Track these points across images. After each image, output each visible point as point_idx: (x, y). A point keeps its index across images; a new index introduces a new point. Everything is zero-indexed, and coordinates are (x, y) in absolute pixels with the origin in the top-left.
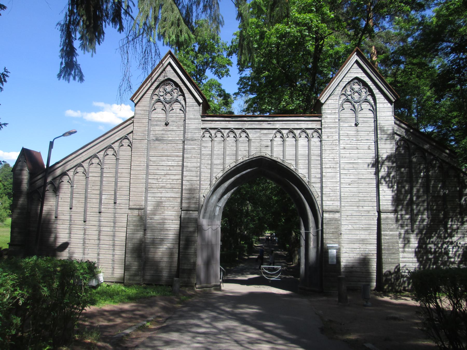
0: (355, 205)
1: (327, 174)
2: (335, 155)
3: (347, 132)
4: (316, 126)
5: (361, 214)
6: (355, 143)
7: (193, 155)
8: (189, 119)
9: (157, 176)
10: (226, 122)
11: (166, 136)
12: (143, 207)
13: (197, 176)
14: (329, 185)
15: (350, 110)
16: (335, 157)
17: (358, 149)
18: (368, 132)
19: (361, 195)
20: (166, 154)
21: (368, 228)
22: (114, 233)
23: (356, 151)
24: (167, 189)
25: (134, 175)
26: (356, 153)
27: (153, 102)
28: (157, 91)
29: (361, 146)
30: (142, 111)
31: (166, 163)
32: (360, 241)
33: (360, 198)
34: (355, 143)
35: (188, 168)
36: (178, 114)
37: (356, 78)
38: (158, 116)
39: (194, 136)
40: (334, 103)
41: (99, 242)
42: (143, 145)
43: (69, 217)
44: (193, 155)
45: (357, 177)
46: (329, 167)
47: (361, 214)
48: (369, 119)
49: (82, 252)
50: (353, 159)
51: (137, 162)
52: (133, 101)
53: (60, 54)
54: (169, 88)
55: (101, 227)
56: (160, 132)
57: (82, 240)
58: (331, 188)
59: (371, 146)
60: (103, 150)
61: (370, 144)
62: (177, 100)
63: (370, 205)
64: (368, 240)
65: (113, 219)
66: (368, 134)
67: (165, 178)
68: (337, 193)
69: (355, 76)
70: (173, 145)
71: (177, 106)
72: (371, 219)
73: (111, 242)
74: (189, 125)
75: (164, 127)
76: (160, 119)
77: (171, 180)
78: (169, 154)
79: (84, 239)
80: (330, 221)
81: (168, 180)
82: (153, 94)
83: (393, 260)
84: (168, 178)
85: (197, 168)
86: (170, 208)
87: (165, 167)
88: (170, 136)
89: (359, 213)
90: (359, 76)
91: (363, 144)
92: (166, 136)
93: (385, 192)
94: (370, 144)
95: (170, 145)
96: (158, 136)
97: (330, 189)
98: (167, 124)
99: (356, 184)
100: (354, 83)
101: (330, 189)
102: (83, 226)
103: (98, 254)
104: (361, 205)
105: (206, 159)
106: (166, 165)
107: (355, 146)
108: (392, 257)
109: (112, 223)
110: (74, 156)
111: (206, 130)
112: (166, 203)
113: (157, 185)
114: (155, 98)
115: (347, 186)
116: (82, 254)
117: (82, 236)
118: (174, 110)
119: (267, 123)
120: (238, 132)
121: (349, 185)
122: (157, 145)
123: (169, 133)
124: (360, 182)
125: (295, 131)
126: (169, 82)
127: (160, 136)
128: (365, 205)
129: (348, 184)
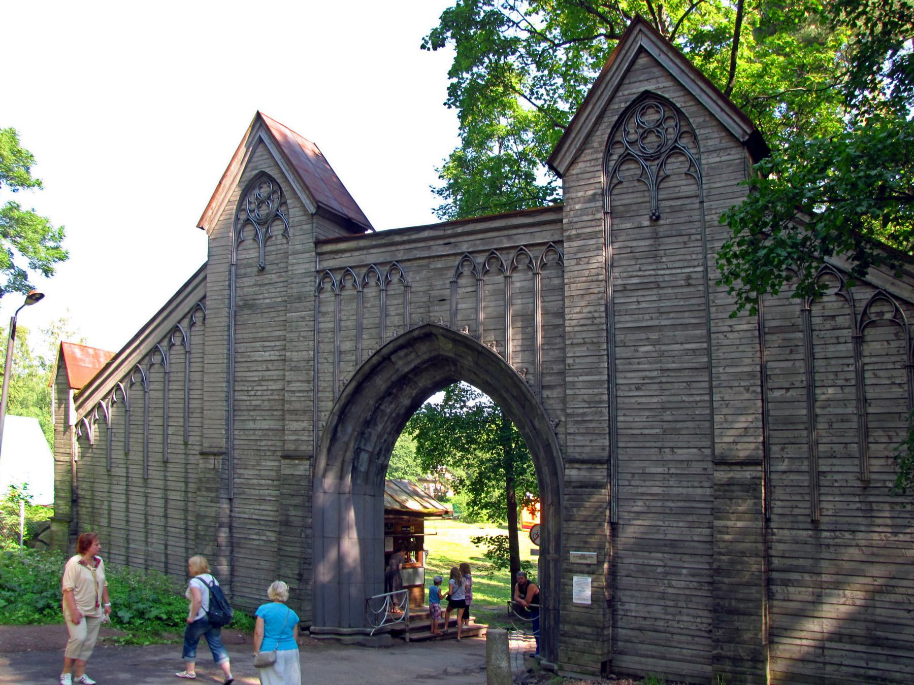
0: (653, 444)
1: (577, 360)
2: (597, 308)
3: (630, 244)
4: (552, 235)
5: (669, 469)
6: (652, 272)
7: (302, 334)
8: (294, 254)
9: (247, 384)
10: (361, 252)
11: (261, 297)
12: (224, 450)
13: (308, 382)
14: (583, 391)
15: (683, 176)
16: (596, 315)
17: (659, 287)
18: (686, 238)
19: (667, 416)
20: (260, 335)
21: (687, 511)
22: (186, 505)
23: (652, 295)
24: (263, 413)
25: (210, 385)
26: (654, 298)
27: (239, 226)
28: (246, 202)
29: (667, 278)
30: (220, 248)
31: (262, 356)
32: (665, 545)
33: (665, 425)
34: (652, 272)
35: (293, 364)
36: (279, 247)
37: (646, 95)
38: (248, 256)
39: (304, 290)
40: (592, 169)
41: (167, 522)
42: (220, 320)
43: (125, 470)
44: (302, 334)
45: (657, 366)
46: (582, 341)
47: (669, 469)
48: (688, 201)
49: (143, 539)
50: (647, 317)
51: (213, 357)
52: (202, 228)
53: (450, 68)
54: (652, 117)
55: (168, 493)
56: (250, 289)
57: (143, 517)
58: (586, 397)
59: (694, 276)
60: (165, 337)
61: (691, 270)
62: (675, 147)
63: (691, 445)
64: (686, 544)
65: (183, 475)
66: (685, 243)
67: (260, 388)
68: (601, 412)
69: (642, 89)
70: (273, 314)
71: (675, 165)
72: (696, 484)
73: (182, 522)
74: (295, 268)
75: (257, 278)
76: (250, 261)
77: (269, 393)
78: (265, 334)
79: (146, 515)
80: (581, 487)
81: (265, 393)
82: (611, 142)
83: (742, 606)
84: (265, 388)
85: (308, 361)
86: (268, 453)
87: (259, 364)
88: (266, 295)
89: (663, 466)
90: (651, 87)
91: (674, 271)
92: (261, 297)
93: (727, 405)
94: (691, 270)
95: (266, 315)
96: (248, 298)
97: (585, 401)
98: (262, 270)
99: (655, 387)
100: (643, 109)
101: (585, 401)
102: (142, 490)
103: (166, 546)
104: (667, 445)
105: (326, 340)
106: (260, 359)
107: (652, 279)
108: (741, 596)
109: (183, 485)
110: (128, 351)
111: (324, 274)
112: (263, 443)
113: (248, 403)
114: (618, 151)
115: (631, 394)
116: (144, 544)
117: (143, 508)
118: (274, 238)
119: (441, 242)
120: (383, 271)
121: (637, 389)
122: (246, 317)
123: (264, 289)
124: (664, 380)
125: (502, 257)
126: (652, 102)
127: (251, 297)
128: (680, 445)
129: (633, 387)
